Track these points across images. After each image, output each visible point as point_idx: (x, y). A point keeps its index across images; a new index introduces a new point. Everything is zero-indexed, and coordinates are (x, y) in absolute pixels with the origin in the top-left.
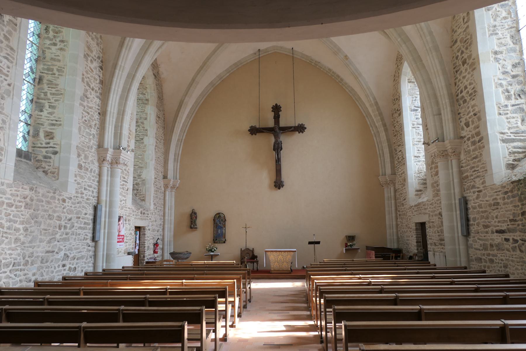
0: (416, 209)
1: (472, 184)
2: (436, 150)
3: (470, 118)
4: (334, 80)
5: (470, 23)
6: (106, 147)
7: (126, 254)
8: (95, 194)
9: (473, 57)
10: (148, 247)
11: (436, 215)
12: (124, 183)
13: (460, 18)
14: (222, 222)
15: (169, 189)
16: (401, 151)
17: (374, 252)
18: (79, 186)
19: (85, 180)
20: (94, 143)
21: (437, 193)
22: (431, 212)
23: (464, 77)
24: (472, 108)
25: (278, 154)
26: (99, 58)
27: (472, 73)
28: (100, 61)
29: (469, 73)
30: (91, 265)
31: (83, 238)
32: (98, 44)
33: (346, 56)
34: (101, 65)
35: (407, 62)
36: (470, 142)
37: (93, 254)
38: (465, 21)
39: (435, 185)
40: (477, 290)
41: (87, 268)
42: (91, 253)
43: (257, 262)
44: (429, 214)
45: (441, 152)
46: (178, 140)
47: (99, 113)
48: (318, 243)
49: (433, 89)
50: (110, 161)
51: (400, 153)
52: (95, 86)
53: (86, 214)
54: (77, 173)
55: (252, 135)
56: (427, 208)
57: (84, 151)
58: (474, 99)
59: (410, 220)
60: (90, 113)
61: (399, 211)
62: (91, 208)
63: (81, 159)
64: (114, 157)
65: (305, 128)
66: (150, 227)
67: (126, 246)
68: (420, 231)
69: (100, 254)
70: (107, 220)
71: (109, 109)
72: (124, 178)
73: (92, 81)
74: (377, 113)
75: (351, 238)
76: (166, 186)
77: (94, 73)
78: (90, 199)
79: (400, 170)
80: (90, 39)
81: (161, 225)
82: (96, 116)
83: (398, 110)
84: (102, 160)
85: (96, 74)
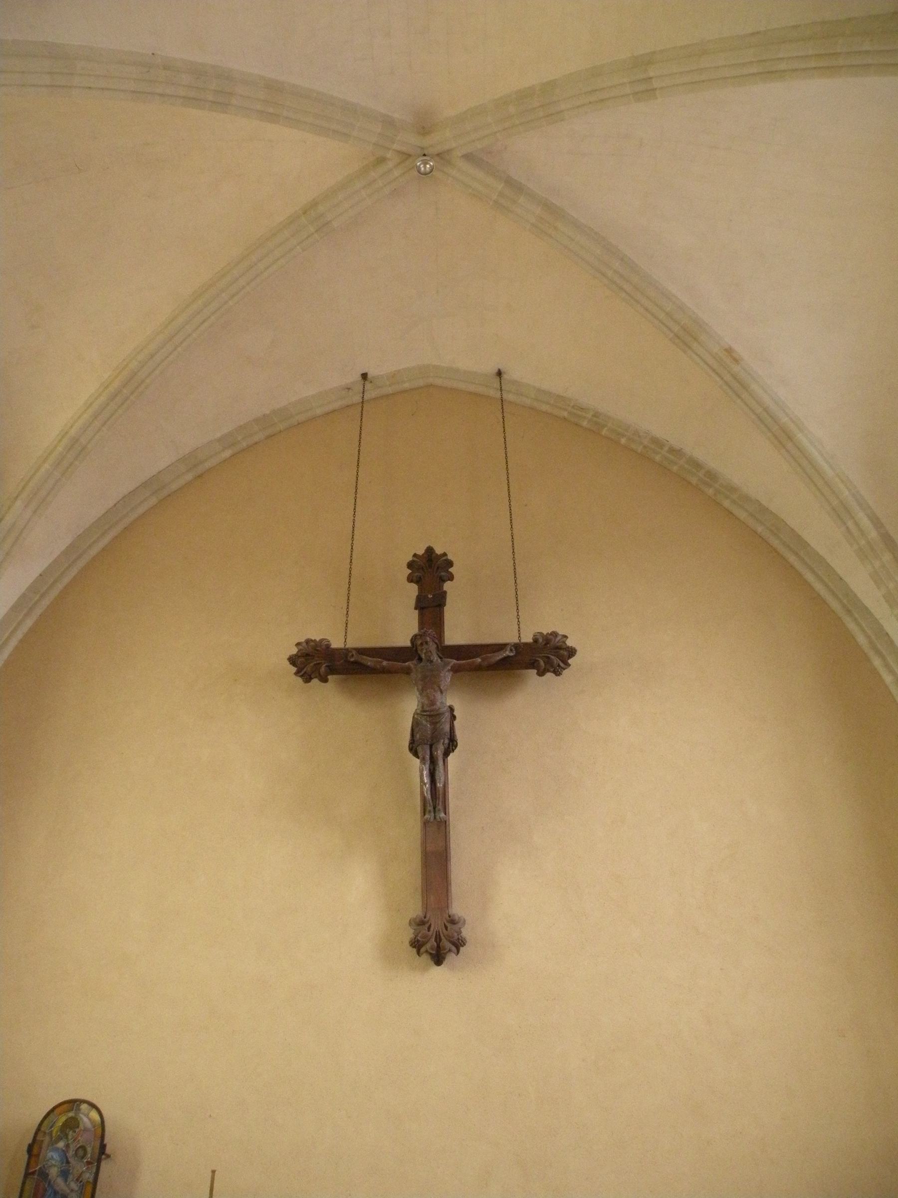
14: (78, 1167)
55: (307, 679)
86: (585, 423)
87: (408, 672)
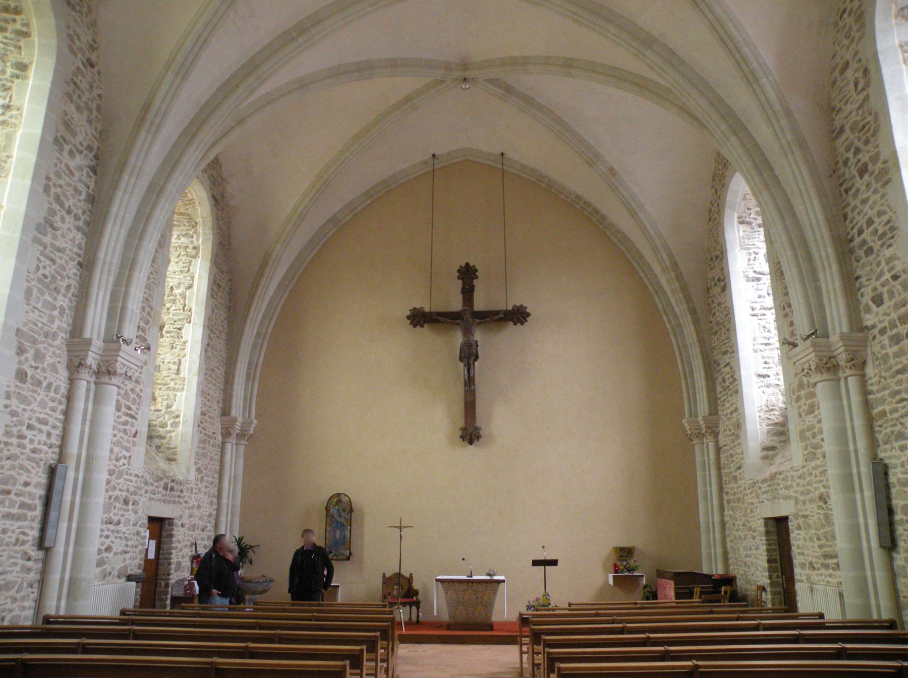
0: (765, 487)
1: (897, 429)
2: (813, 355)
3: (883, 285)
4: (587, 218)
5: (871, 91)
6: (87, 335)
7: (123, 579)
8: (55, 441)
9: (882, 157)
10: (179, 563)
11: (812, 501)
12: (128, 419)
13: (847, 84)
14: (343, 514)
15: (233, 440)
16: (728, 364)
17: (672, 582)
18: (15, 419)
19: (32, 407)
20: (61, 325)
21: (813, 452)
22: (802, 493)
23: (864, 202)
24: (888, 263)
25: (469, 367)
26: (90, 148)
27: (882, 191)
28: (91, 156)
29: (875, 192)
30: (29, 603)
31: (13, 540)
32: (89, 121)
33: (612, 169)
34: (93, 163)
35: (742, 172)
36: (885, 336)
37: (38, 577)
38: (860, 87)
39: (809, 435)
40: (839, 654)
41: (17, 612)
42: (33, 576)
43: (417, 604)
44: (796, 498)
45: (825, 360)
46: (258, 334)
47: (80, 264)
48: (554, 563)
49: (798, 226)
50: (94, 367)
51: (727, 369)
52: (74, 204)
53: (26, 484)
54: (12, 389)
55: (415, 326)
56: (791, 486)
57: (35, 342)
58: (890, 246)
59: (752, 511)
60: (58, 261)
61: (727, 493)
62: (41, 470)
63: (27, 360)
64: (103, 358)
65: (529, 315)
66: (185, 520)
67: (124, 560)
68: (775, 538)
69: (55, 577)
70: (78, 499)
71: (101, 255)
72: (129, 408)
73: (68, 194)
74: (677, 285)
75: (625, 553)
76: (226, 434)
77: (76, 179)
78: (41, 451)
79: (727, 405)
80: (72, 109)
81: (210, 515)
82: (72, 269)
83: (719, 280)
84: (75, 366)
85: (80, 181)
86: (544, 185)
87: (458, 324)
